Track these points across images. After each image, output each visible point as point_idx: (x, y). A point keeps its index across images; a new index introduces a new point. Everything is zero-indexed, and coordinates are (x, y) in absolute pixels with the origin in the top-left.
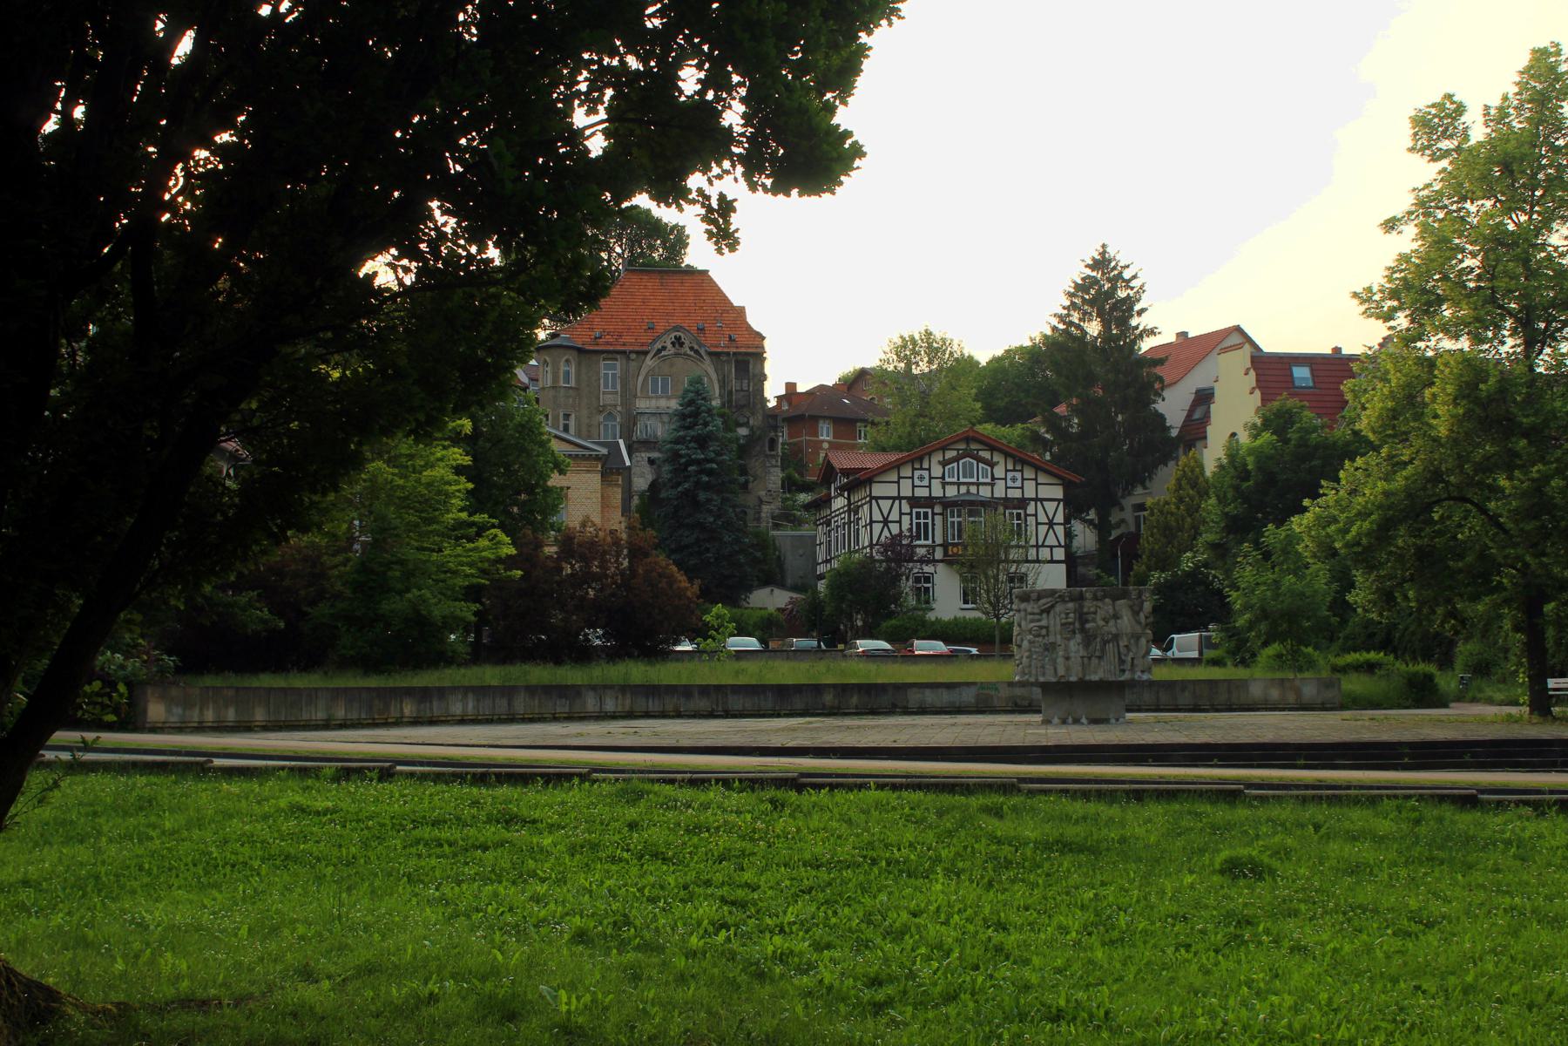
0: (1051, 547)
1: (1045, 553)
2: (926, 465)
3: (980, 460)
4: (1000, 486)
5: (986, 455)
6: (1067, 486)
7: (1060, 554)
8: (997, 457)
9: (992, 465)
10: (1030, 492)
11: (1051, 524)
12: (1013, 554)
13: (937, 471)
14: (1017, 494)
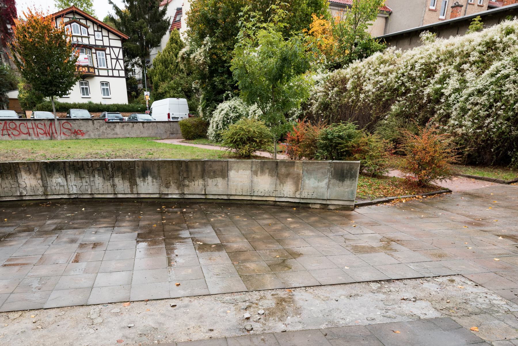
0: (119, 70)
1: (116, 73)
3: (81, 24)
4: (92, 38)
5: (83, 22)
6: (123, 41)
7: (122, 73)
8: (89, 24)
9: (87, 28)
10: (106, 43)
11: (117, 59)
12: (102, 73)
14: (99, 43)
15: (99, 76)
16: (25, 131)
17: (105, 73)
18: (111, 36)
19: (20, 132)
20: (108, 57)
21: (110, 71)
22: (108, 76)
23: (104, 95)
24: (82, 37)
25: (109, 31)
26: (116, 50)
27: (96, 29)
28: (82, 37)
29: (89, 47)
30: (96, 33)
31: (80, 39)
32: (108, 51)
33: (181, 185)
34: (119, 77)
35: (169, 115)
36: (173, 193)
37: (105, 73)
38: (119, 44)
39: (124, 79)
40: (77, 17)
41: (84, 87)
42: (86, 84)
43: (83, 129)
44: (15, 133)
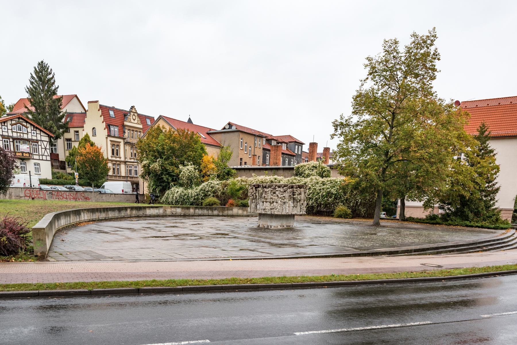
1: (44, 158)
2: (6, 125)
3: (23, 125)
4: (30, 135)
5: (25, 124)
8: (28, 125)
9: (27, 128)
10: (39, 138)
11: (46, 149)
13: (10, 127)
15: (33, 159)
16: (65, 197)
17: (37, 157)
18: (42, 134)
19: (63, 197)
20: (40, 147)
21: (41, 156)
22: (39, 160)
23: (36, 172)
24: (23, 133)
25: (41, 130)
26: (45, 143)
27: (32, 129)
28: (23, 133)
29: (28, 140)
30: (33, 131)
31: (22, 135)
32: (39, 143)
33: (223, 212)
34: (47, 160)
35: (25, 184)
36: (221, 214)
37: (37, 157)
38: (47, 139)
39: (50, 162)
40: (21, 120)
41: (23, 166)
42: (25, 164)
43: (90, 197)
44: (61, 198)
